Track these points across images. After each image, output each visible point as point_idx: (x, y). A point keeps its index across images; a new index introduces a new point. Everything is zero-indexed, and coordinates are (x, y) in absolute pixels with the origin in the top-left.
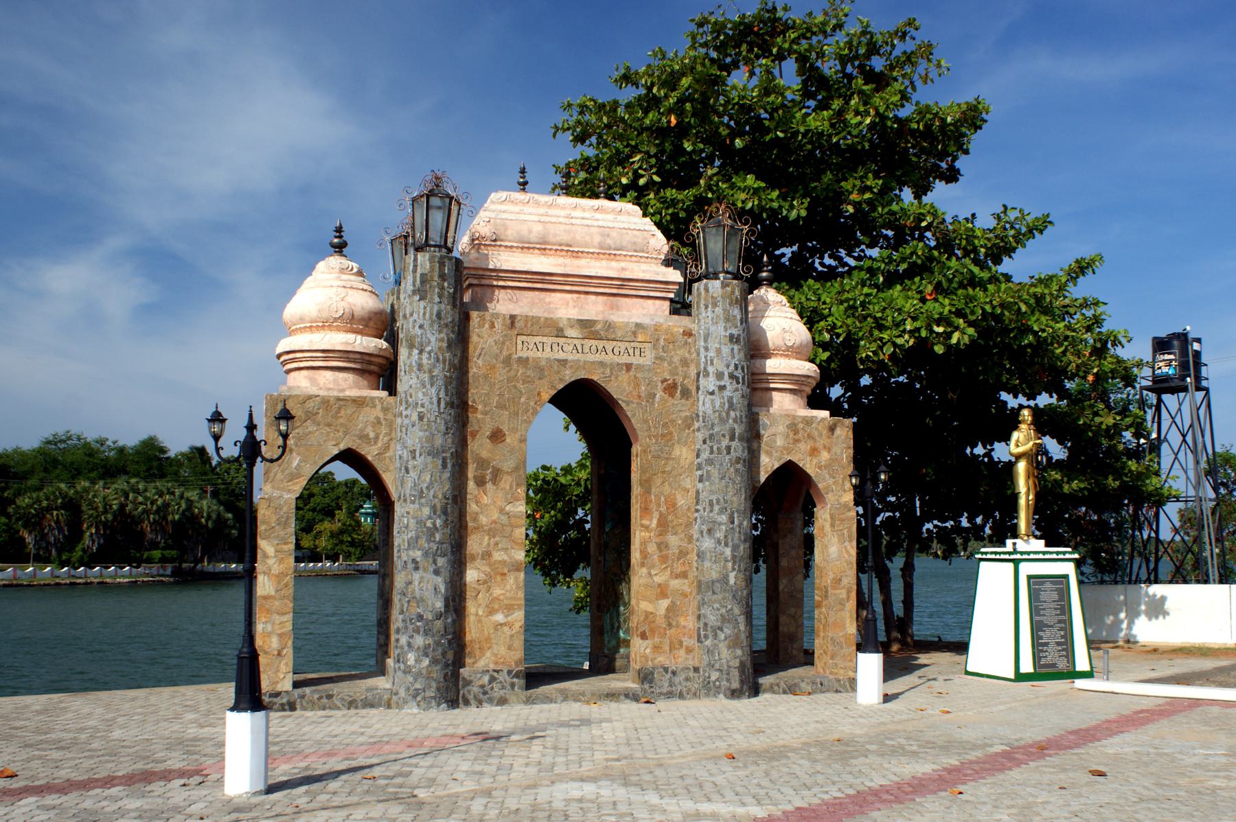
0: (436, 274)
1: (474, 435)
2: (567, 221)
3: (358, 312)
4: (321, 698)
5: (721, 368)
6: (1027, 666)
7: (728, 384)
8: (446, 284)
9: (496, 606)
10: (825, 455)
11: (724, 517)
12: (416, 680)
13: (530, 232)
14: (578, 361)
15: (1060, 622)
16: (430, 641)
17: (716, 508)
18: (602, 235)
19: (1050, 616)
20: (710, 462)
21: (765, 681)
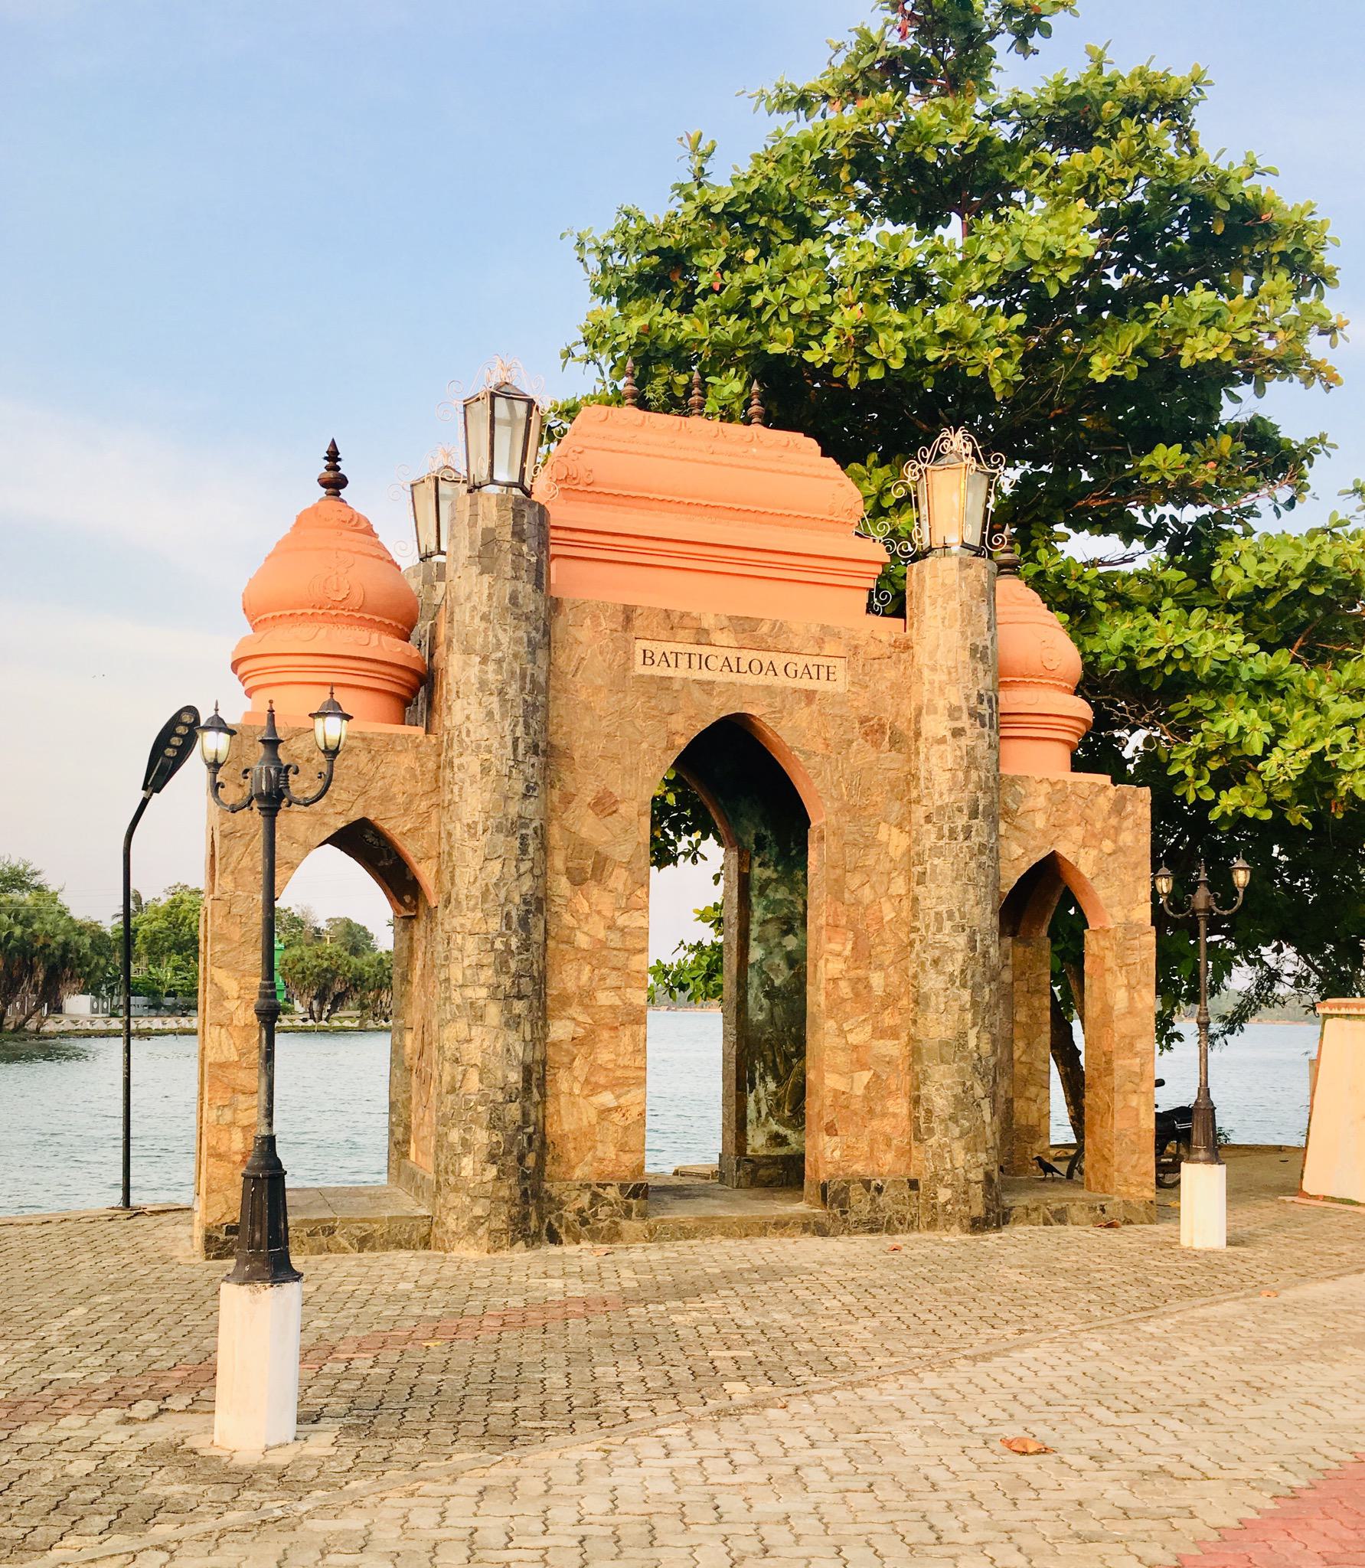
0: (506, 533)
8: (525, 548)
16: (498, 1137)
17: (948, 925)
21: (1019, 1201)
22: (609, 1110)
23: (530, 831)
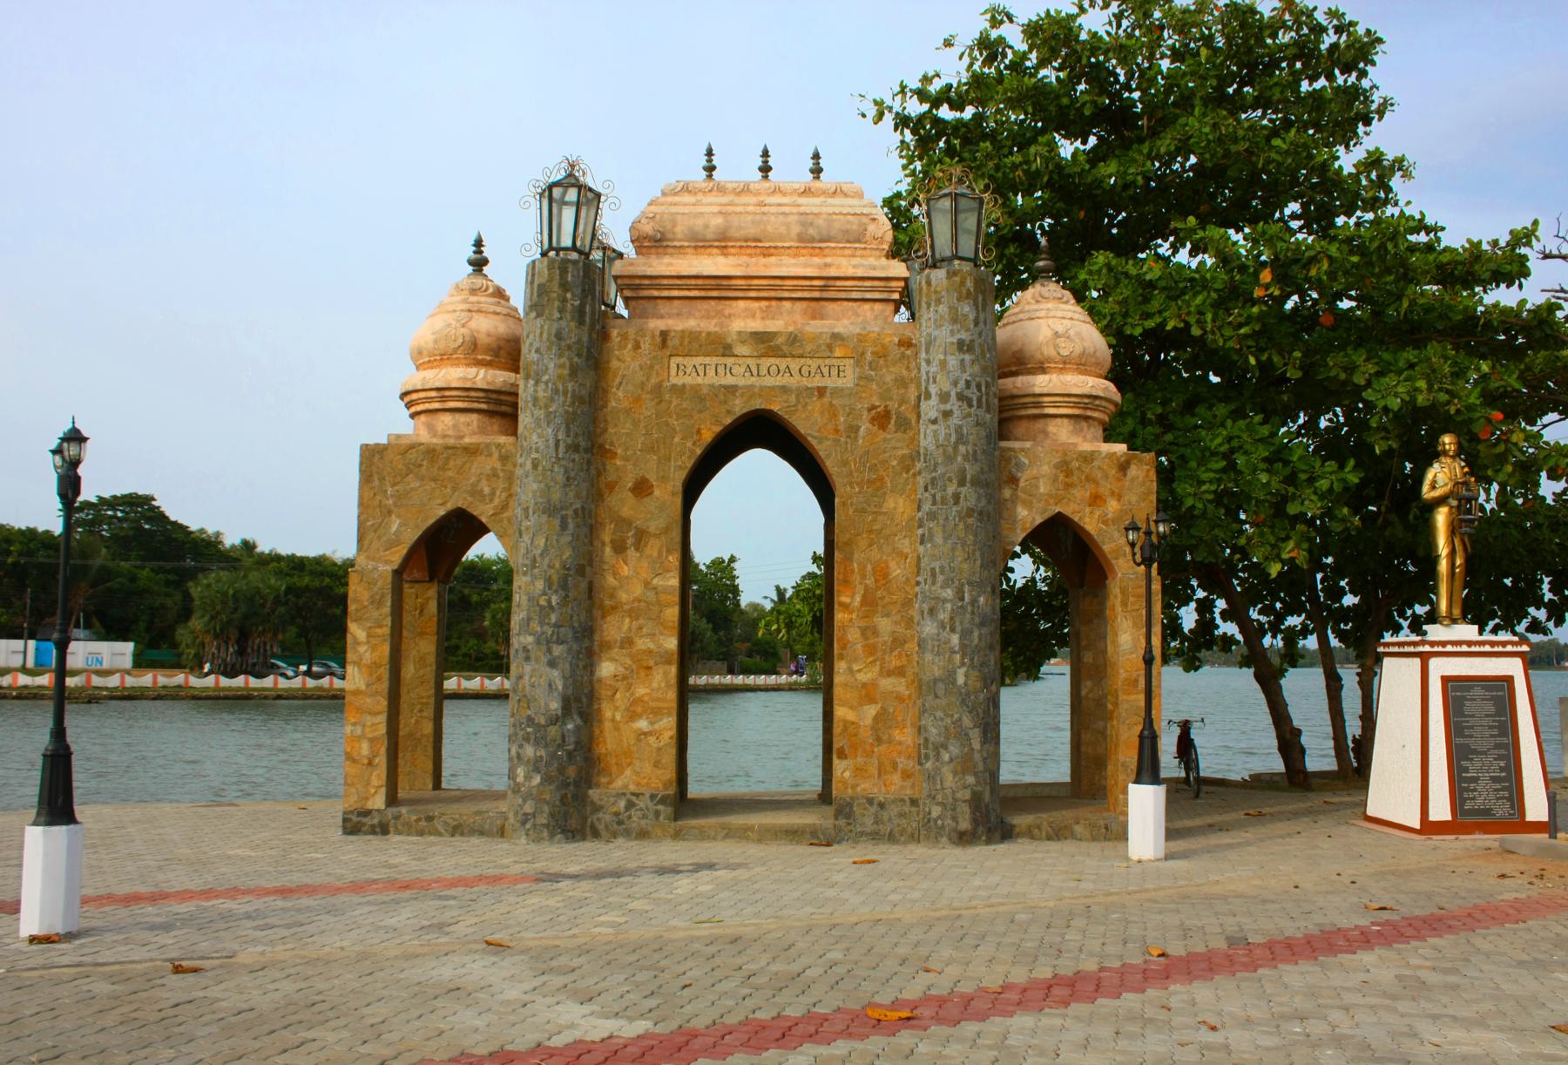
0: (555, 286)
1: (611, 487)
2: (758, 209)
3: (483, 340)
4: (419, 820)
5: (946, 387)
6: (1441, 810)
7: (955, 408)
9: (639, 710)
10: (1113, 505)
11: (949, 591)
12: (525, 801)
13: (707, 226)
14: (752, 386)
15: (1497, 746)
16: (542, 752)
17: (940, 578)
18: (803, 224)
19: (1482, 738)
20: (932, 516)
22: (645, 734)
23: (570, 512)
